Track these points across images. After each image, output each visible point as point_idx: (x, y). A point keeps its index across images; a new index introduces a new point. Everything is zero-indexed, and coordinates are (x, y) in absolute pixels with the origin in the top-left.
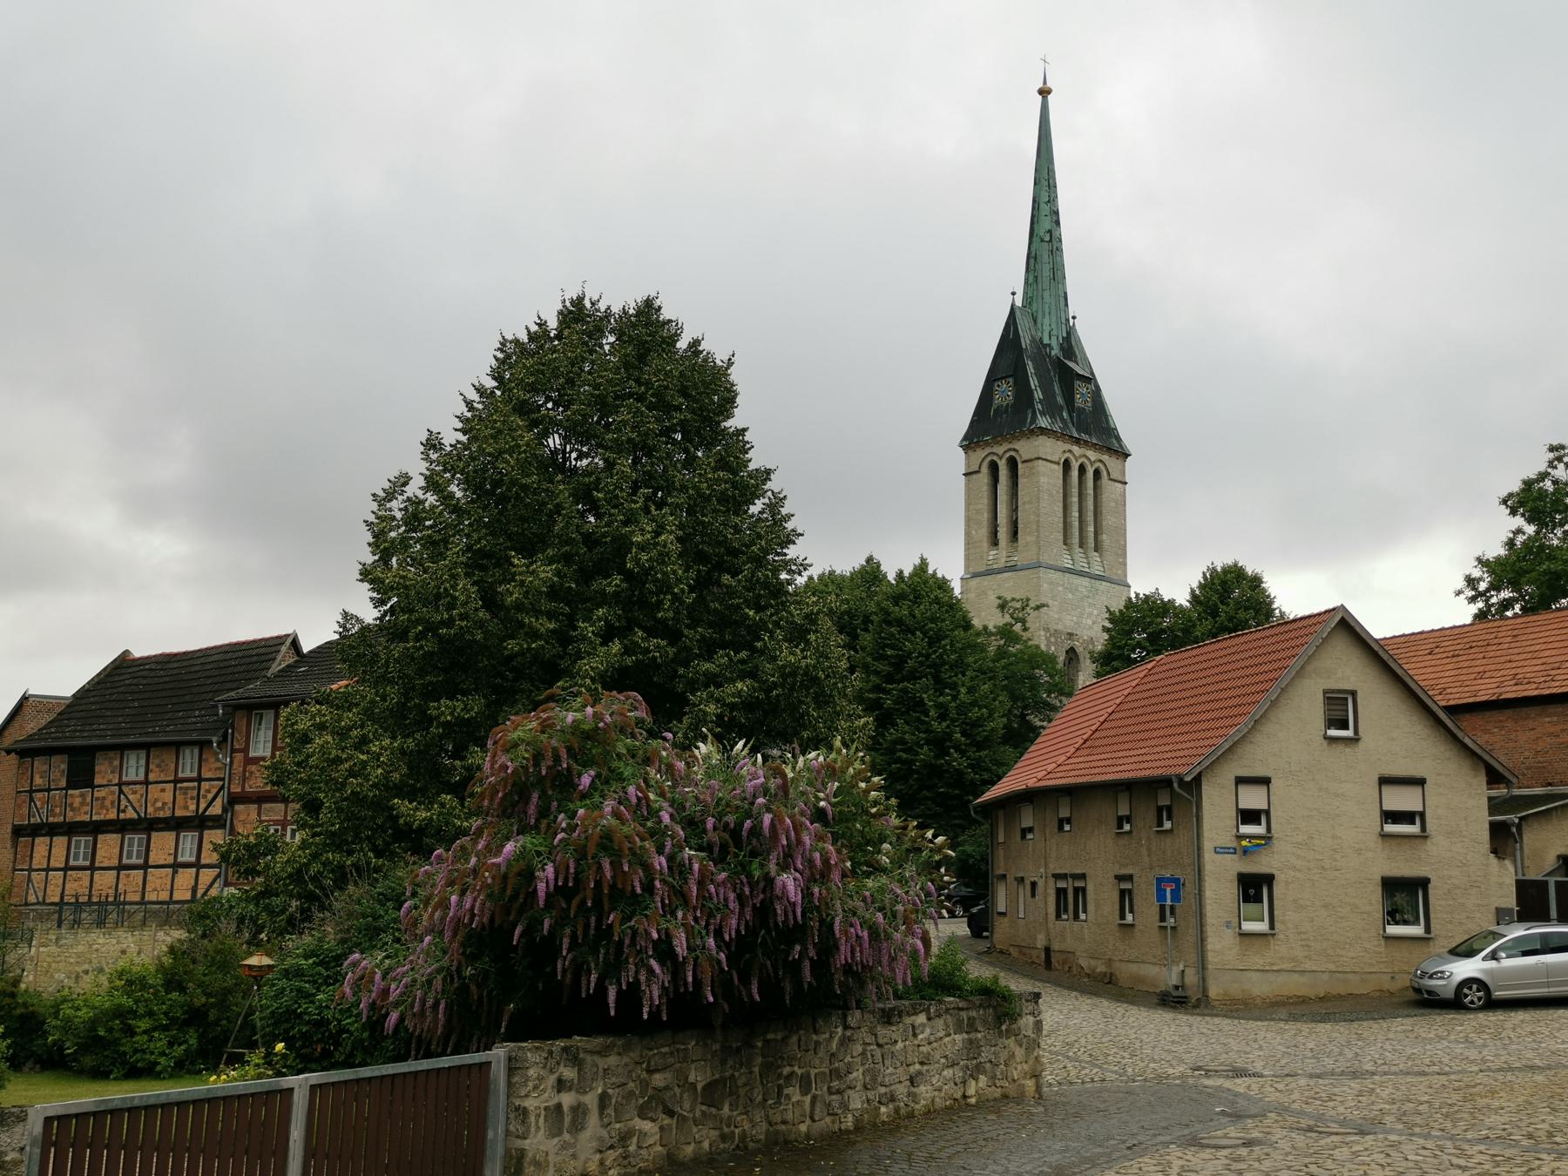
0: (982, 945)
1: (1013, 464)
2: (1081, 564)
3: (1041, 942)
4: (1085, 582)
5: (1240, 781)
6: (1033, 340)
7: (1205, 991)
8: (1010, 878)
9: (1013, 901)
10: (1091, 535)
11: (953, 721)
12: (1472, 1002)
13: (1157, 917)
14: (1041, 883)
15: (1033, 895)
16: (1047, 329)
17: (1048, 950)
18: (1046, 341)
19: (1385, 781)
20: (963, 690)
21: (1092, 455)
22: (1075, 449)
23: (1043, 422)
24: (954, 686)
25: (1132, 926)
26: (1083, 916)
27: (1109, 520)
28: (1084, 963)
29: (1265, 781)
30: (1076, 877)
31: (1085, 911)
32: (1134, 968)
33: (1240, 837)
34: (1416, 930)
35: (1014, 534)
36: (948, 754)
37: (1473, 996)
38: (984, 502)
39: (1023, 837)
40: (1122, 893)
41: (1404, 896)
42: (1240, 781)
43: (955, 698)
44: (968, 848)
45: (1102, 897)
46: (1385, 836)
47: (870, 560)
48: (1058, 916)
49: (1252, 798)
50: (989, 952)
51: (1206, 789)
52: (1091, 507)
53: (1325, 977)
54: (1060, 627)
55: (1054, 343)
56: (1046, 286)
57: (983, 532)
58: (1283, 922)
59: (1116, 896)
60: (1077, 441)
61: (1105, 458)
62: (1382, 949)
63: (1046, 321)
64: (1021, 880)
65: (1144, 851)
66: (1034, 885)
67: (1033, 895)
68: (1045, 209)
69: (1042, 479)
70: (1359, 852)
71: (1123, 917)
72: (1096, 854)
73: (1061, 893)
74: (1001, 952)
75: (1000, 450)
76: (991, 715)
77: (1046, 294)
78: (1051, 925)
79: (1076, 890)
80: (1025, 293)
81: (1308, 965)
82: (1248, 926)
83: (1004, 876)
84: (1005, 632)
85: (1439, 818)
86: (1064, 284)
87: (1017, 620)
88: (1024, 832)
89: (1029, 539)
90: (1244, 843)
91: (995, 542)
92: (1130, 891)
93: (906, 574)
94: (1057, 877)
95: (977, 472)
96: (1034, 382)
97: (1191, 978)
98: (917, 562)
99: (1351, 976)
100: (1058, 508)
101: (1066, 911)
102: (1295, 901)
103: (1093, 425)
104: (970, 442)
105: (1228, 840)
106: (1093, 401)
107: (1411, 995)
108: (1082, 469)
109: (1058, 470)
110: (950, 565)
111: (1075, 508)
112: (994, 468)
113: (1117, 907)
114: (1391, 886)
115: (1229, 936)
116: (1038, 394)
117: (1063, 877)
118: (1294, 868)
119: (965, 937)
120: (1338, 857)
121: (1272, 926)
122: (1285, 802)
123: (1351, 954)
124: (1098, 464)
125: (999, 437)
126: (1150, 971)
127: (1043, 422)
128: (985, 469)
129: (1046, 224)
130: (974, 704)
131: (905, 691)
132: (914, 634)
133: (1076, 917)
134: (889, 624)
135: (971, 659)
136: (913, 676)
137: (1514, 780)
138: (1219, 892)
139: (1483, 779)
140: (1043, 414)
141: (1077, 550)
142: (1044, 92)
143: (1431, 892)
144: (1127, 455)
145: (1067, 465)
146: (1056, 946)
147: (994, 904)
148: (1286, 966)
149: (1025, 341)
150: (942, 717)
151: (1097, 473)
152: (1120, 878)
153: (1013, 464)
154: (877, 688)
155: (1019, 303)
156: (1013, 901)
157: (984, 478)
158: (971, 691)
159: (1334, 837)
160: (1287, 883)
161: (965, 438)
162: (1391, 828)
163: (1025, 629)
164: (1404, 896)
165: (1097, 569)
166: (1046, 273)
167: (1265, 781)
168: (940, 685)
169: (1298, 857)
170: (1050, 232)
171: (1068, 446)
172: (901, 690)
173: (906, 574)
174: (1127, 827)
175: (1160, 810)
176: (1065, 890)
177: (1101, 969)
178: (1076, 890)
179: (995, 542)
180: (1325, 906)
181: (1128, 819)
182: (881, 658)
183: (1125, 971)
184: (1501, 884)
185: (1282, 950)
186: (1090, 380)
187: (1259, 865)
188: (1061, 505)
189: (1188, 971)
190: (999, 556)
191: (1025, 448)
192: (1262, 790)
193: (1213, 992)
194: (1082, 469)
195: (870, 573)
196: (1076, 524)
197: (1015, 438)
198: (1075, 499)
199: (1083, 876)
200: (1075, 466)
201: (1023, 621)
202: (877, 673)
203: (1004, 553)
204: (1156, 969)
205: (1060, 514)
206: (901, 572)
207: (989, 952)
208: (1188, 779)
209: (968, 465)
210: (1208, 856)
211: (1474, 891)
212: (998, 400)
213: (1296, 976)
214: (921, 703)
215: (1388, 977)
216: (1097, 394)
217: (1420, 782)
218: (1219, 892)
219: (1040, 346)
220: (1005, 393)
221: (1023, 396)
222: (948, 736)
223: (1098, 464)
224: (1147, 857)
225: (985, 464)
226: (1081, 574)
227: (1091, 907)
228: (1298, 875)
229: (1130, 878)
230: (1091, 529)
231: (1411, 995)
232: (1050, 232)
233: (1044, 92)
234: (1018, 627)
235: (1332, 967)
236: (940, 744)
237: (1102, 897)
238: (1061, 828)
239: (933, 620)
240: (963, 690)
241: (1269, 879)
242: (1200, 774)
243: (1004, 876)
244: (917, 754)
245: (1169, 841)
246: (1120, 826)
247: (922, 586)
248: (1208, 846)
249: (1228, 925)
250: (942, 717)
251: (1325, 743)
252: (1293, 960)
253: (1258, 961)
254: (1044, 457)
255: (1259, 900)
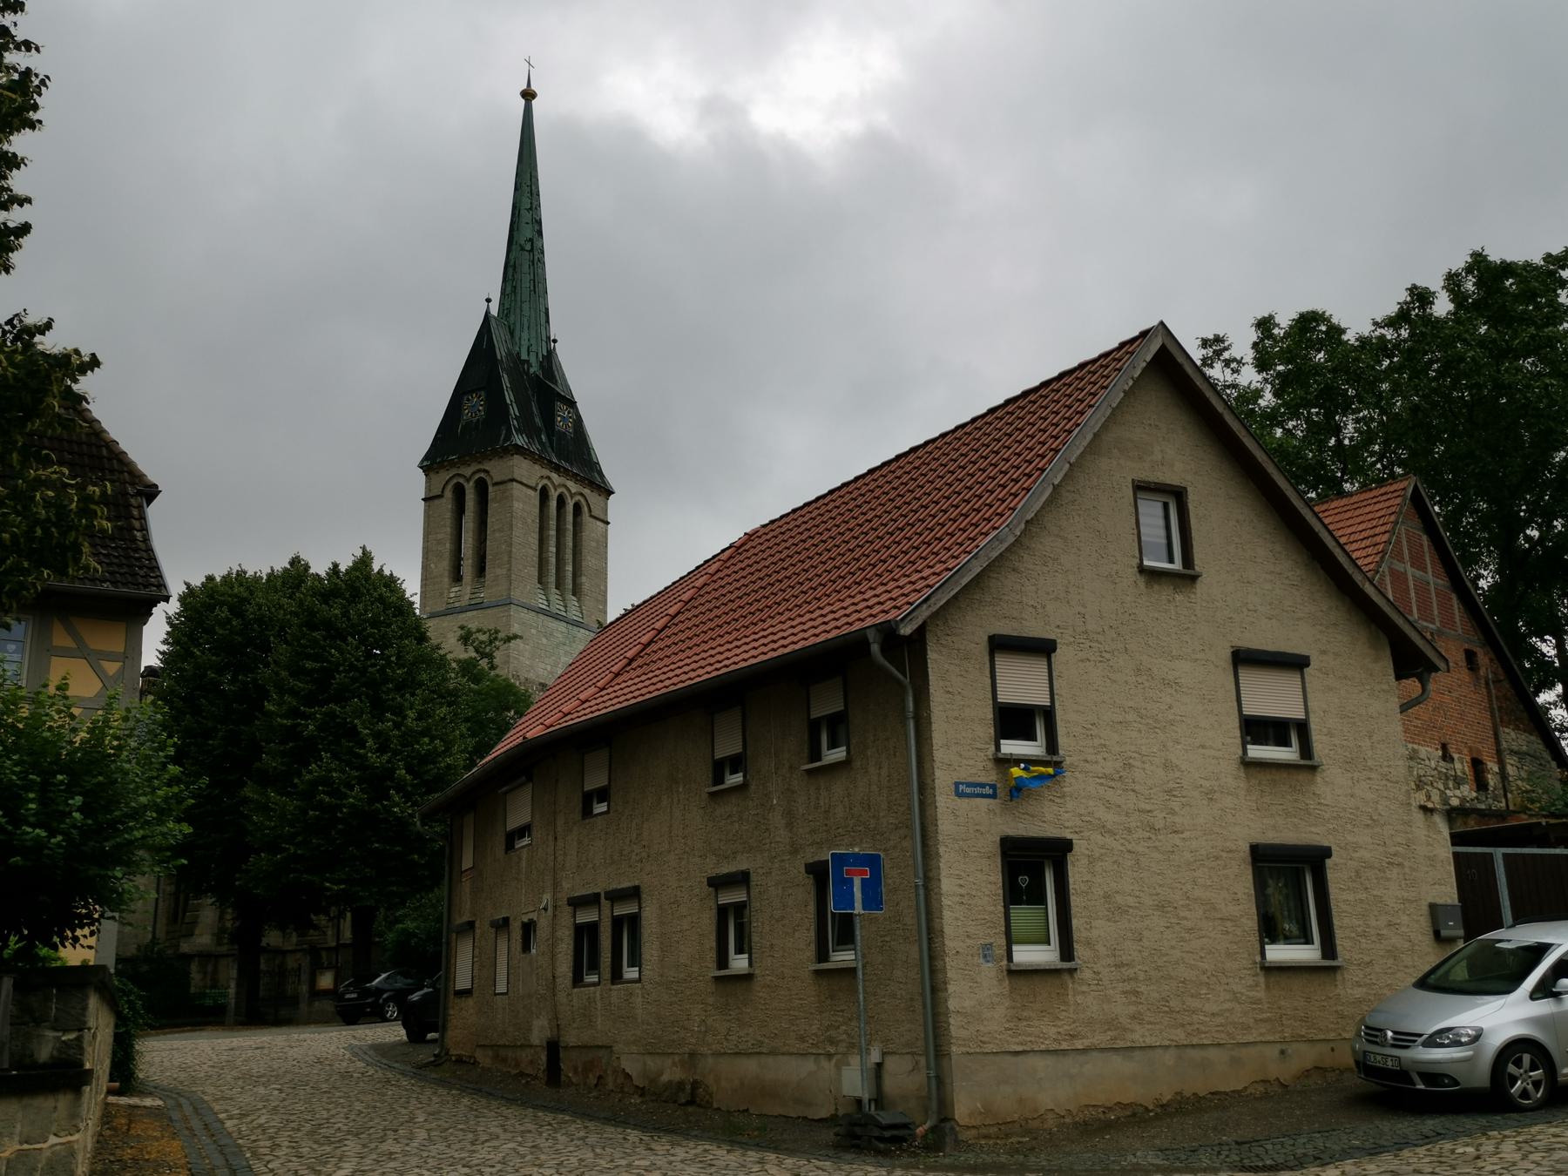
0: (425, 1054)
1: (482, 488)
2: (557, 606)
3: (539, 1032)
4: (562, 626)
5: (1001, 645)
6: (509, 354)
7: (945, 1116)
8: (483, 927)
9: (486, 965)
10: (569, 575)
11: (395, 753)
12: (1525, 1094)
13: (811, 952)
14: (543, 923)
15: (526, 947)
16: (525, 343)
17: (553, 1047)
18: (524, 356)
19: (1243, 659)
20: (411, 714)
21: (573, 487)
22: (554, 476)
23: (520, 440)
24: (399, 711)
25: (747, 978)
26: (631, 973)
27: (589, 561)
28: (630, 1065)
29: (1043, 649)
30: (616, 896)
31: (635, 961)
32: (750, 1066)
33: (1004, 762)
34: (1306, 954)
35: (481, 570)
36: (388, 798)
37: (1525, 1080)
38: (446, 531)
39: (510, 846)
40: (722, 911)
41: (1290, 882)
42: (1001, 645)
43: (397, 726)
44: (410, 925)
45: (677, 928)
46: (1249, 765)
47: (295, 561)
48: (577, 980)
49: (1022, 683)
50: (436, 1063)
51: (937, 660)
52: (570, 544)
53: (1169, 1058)
54: (531, 676)
55: (533, 360)
56: (526, 296)
57: (444, 565)
58: (1088, 943)
59: (708, 921)
60: (556, 468)
61: (587, 491)
62: (1260, 993)
63: (525, 335)
64: (503, 925)
65: (777, 819)
66: (528, 929)
67: (526, 947)
68: (526, 216)
69: (516, 504)
70: (1209, 796)
71: (723, 962)
72: (666, 848)
73: (586, 935)
74: (460, 1061)
75: (467, 471)
76: (448, 749)
77: (526, 306)
78: (562, 997)
79: (617, 922)
80: (501, 304)
81: (1139, 1036)
82: (1026, 955)
83: (471, 925)
84: (467, 667)
85: (1330, 734)
86: (546, 299)
87: (484, 655)
88: (511, 838)
89: (499, 571)
90: (1016, 772)
91: (457, 578)
92: (740, 908)
93: (343, 568)
94: (577, 903)
95: (440, 496)
96: (509, 397)
97: (903, 1077)
98: (359, 553)
99: (1212, 1053)
100: (534, 540)
101: (594, 966)
102: (1107, 897)
103: (572, 454)
104: (431, 464)
105: (978, 768)
106: (575, 431)
107: (1355, 1081)
108: (561, 501)
109: (535, 497)
110: (405, 566)
111: (553, 542)
112: (459, 492)
113: (711, 942)
114: (1265, 859)
115: (989, 973)
116: (510, 419)
117: (592, 900)
118: (1104, 829)
119: (401, 1044)
120: (1175, 805)
121: (1067, 952)
122: (1082, 693)
123: (1211, 1007)
124: (578, 498)
125: (466, 457)
126: (792, 1070)
127: (520, 440)
128: (449, 494)
129: (527, 232)
130: (425, 732)
131: (332, 715)
132: (344, 640)
133: (617, 976)
134: (314, 628)
135: (424, 676)
136: (341, 697)
137: (1442, 665)
138: (968, 883)
139: (1387, 665)
140: (519, 431)
141: (554, 590)
142: (528, 95)
143: (1331, 876)
144: (610, 492)
145: (544, 494)
146: (571, 1038)
147: (449, 977)
148: (1101, 1039)
149: (501, 352)
150: (382, 749)
151: (577, 507)
152: (719, 883)
153: (482, 488)
154: (294, 713)
155: (494, 311)
156: (486, 965)
157: (446, 504)
158: (421, 716)
159: (1168, 766)
160: (1092, 860)
161: (426, 458)
162: (1257, 752)
163: (493, 667)
164: (1290, 882)
165: (574, 614)
166: (526, 283)
167: (1043, 649)
168: (379, 708)
169: (1108, 805)
170: (531, 240)
171: (546, 472)
172: (325, 714)
173: (343, 568)
174: (735, 779)
175: (814, 727)
176: (593, 928)
177: (671, 1073)
178: (617, 922)
179: (457, 578)
180: (1161, 907)
181: (736, 763)
182: (298, 672)
183: (728, 1075)
184: (1432, 860)
185: (1093, 999)
186: (572, 404)
187: (1042, 821)
188: (536, 536)
189: (891, 1064)
190: (464, 593)
191: (497, 469)
192: (1037, 667)
193: (963, 1108)
194: (561, 501)
195: (297, 571)
196: (553, 560)
197: (485, 457)
198: (553, 533)
199: (634, 893)
200: (554, 495)
201: (490, 656)
202: (293, 692)
203: (468, 589)
204: (809, 1065)
205: (535, 547)
206: (336, 566)
207: (436, 1063)
208: (906, 630)
209: (428, 488)
210: (944, 801)
211: (1394, 873)
212: (467, 414)
213: (1117, 1061)
214: (353, 733)
215: (1273, 1052)
216: (579, 422)
217: (1296, 664)
218: (968, 883)
219: (518, 364)
220: (476, 407)
221: (497, 409)
222: (388, 773)
223: (578, 498)
224: (783, 827)
225: (450, 487)
226: (556, 617)
227: (650, 951)
228: (1108, 840)
229: (742, 879)
230: (569, 568)
231: (1355, 1081)
232: (531, 240)
233: (528, 95)
234: (484, 663)
235: (1180, 1036)
236: (379, 783)
237: (677, 928)
238: (587, 812)
239: (375, 623)
240: (411, 714)
241: (1057, 851)
242: (925, 623)
243: (471, 925)
244: (346, 796)
245: (839, 787)
246: (718, 779)
247: (362, 585)
248: (943, 779)
249: (986, 951)
250: (382, 749)
251: (1141, 581)
252: (1111, 1023)
253: (1047, 1031)
254: (523, 481)
255: (1040, 899)
